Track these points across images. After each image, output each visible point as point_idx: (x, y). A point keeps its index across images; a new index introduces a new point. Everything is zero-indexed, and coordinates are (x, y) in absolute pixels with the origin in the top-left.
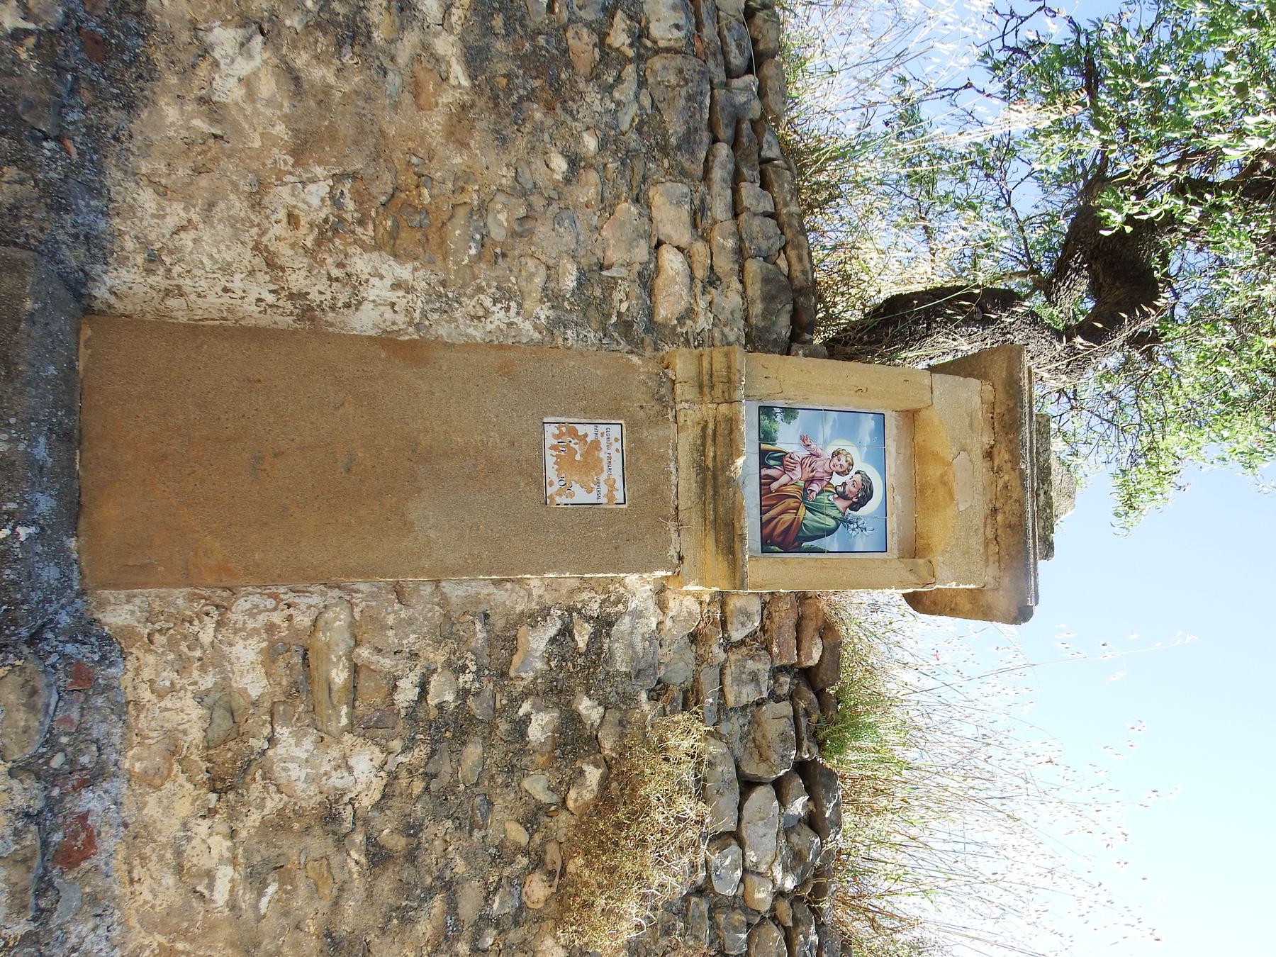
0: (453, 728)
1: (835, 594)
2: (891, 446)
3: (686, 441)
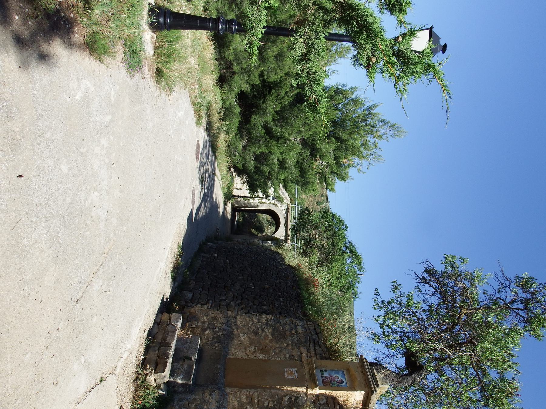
1: (42, 6)
2: (346, 375)
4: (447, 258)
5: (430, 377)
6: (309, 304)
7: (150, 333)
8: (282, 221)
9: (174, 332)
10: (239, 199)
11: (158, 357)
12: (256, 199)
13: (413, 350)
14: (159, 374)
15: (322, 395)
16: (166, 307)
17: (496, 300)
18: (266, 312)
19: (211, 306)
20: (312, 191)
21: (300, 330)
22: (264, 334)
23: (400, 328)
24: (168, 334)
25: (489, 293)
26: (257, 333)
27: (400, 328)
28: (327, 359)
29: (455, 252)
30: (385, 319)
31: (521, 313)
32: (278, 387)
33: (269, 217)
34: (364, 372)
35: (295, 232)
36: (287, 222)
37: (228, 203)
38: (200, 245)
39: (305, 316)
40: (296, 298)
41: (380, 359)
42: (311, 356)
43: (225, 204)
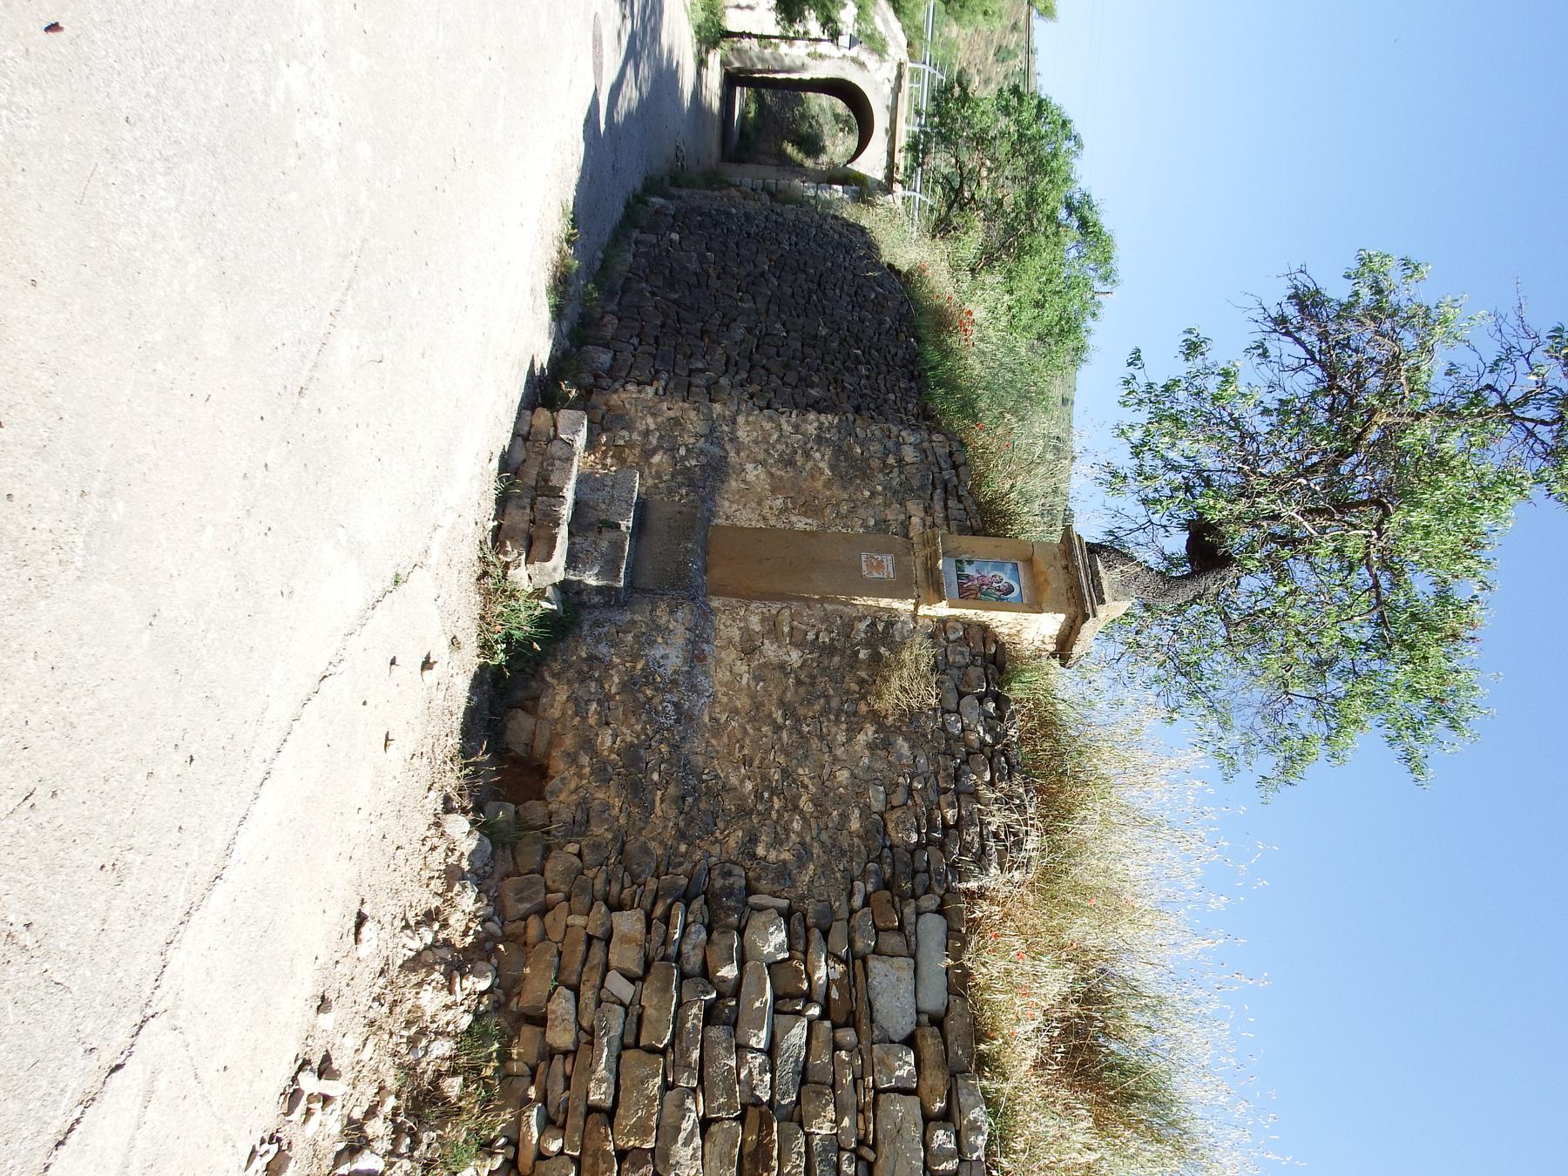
0: (830, 650)
2: (1021, 573)
3: (919, 562)
4: (1365, 261)
5: (1248, 583)
6: (939, 384)
7: (506, 463)
8: (881, 121)
9: (569, 460)
10: (746, 43)
11: (533, 522)
12: (797, 43)
13: (1213, 517)
14: (537, 564)
15: (956, 619)
16: (542, 392)
17: (1477, 393)
18: (818, 407)
19: (665, 390)
20: (980, 17)
21: (909, 454)
22: (808, 467)
23: (1187, 458)
24: (553, 465)
25: (1464, 372)
26: (790, 463)
27: (1187, 458)
28: (975, 532)
29: (1389, 244)
30: (1147, 432)
31: (1543, 432)
32: (843, 598)
33: (840, 106)
34: (1069, 568)
35: (915, 159)
36: (893, 122)
37: (711, 56)
38: (628, 206)
39: (927, 418)
40: (904, 366)
41: (1121, 533)
42: (934, 525)
43: (702, 63)
